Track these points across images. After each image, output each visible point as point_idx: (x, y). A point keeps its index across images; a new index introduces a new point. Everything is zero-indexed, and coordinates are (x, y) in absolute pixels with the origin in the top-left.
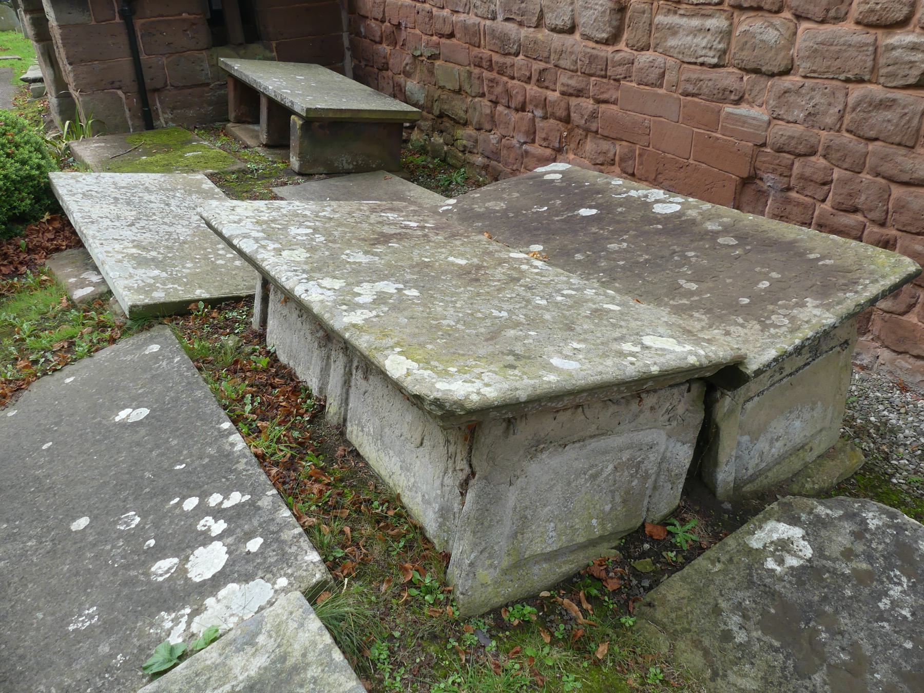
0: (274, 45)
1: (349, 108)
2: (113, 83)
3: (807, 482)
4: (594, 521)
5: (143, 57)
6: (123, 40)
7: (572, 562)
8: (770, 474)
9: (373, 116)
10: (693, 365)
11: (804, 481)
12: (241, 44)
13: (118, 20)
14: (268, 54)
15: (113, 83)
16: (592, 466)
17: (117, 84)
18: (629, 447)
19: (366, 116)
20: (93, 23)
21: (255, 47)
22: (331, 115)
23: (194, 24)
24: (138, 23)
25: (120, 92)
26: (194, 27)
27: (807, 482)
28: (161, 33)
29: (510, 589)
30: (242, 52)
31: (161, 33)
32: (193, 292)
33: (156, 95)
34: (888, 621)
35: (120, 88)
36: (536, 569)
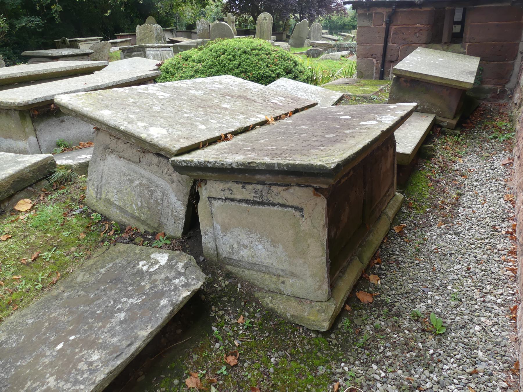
0: (467, 45)
1: (420, 72)
2: (372, 55)
3: (268, 298)
4: (134, 206)
5: (390, 44)
6: (383, 35)
7: (128, 220)
8: (246, 272)
9: (436, 80)
10: (141, 137)
11: (267, 296)
12: (445, 43)
13: (384, 25)
14: (462, 50)
15: (372, 55)
16: (129, 175)
17: (374, 56)
18: (148, 179)
19: (431, 79)
20: (373, 26)
21: (457, 46)
22: (407, 74)
23: (421, 30)
24: (393, 28)
25: (374, 60)
26: (421, 31)
27: (268, 298)
28: (403, 33)
29: (101, 207)
30: (445, 47)
31: (403, 33)
32: (177, 94)
33: (392, 64)
34: (114, 303)
35: (375, 58)
36: (114, 210)
